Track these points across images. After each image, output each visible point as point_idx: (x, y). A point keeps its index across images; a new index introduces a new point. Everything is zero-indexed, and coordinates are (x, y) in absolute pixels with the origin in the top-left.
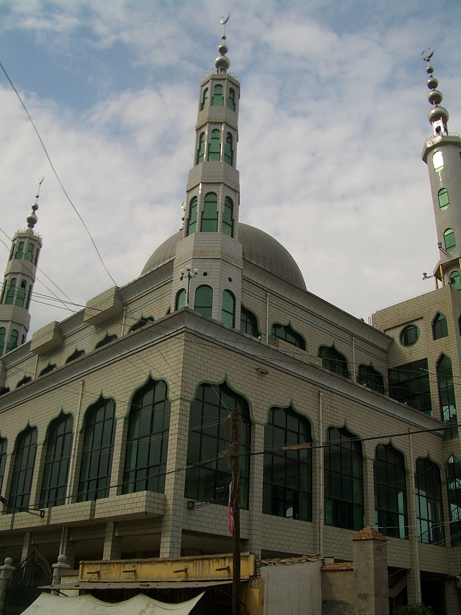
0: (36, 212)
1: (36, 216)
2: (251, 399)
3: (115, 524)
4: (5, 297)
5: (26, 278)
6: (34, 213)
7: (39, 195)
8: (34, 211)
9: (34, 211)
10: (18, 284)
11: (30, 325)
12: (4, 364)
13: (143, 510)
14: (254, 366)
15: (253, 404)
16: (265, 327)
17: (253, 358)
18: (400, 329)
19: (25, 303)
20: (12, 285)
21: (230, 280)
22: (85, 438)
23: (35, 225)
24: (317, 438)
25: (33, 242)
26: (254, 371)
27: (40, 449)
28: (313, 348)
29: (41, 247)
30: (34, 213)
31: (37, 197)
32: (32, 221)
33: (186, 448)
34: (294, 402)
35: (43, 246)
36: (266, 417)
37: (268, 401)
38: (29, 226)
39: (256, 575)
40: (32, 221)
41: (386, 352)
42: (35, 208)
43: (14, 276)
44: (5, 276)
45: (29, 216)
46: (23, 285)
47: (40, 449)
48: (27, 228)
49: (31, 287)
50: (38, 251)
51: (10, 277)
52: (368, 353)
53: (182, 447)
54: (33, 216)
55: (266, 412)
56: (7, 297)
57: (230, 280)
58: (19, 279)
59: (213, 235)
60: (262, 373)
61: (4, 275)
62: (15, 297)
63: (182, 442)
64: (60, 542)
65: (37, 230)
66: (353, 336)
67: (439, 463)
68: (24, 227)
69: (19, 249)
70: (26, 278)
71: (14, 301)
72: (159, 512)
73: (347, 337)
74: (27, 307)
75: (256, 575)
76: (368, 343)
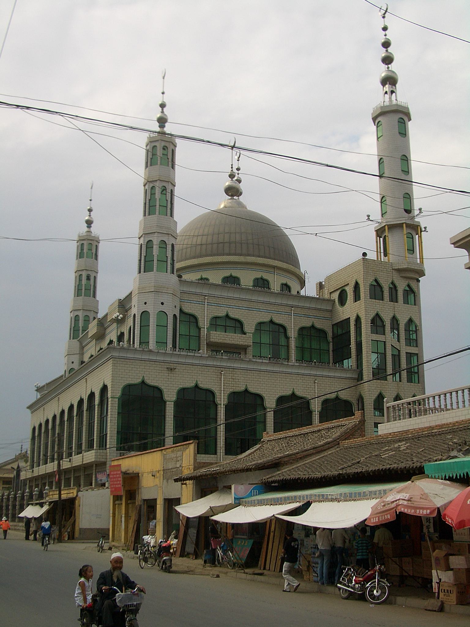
0: (165, 109)
1: (165, 115)
2: (162, 387)
3: (96, 465)
4: (147, 208)
5: (89, 273)
6: (162, 112)
7: (165, 91)
8: (162, 110)
9: (162, 110)
10: (158, 191)
13: (93, 460)
14: (165, 367)
16: (204, 323)
17: (164, 362)
18: (338, 292)
19: (169, 211)
21: (162, 304)
22: (101, 408)
24: (219, 402)
25: (90, 242)
26: (166, 369)
28: (249, 327)
29: (176, 146)
30: (162, 112)
31: (163, 93)
33: (116, 424)
34: (199, 382)
35: (178, 146)
36: (175, 396)
37: (177, 386)
38: (88, 227)
40: (89, 223)
41: (331, 311)
42: (163, 106)
43: (80, 273)
44: (144, 186)
48: (87, 229)
49: (172, 192)
50: (173, 152)
51: (149, 186)
53: (113, 424)
54: (163, 115)
55: (175, 393)
56: (150, 207)
57: (162, 304)
61: (143, 185)
63: (113, 421)
64: (71, 478)
65: (95, 229)
66: (292, 307)
67: (351, 399)
69: (153, 155)
70: (89, 273)
71: (157, 211)
72: (103, 460)
73: (287, 309)
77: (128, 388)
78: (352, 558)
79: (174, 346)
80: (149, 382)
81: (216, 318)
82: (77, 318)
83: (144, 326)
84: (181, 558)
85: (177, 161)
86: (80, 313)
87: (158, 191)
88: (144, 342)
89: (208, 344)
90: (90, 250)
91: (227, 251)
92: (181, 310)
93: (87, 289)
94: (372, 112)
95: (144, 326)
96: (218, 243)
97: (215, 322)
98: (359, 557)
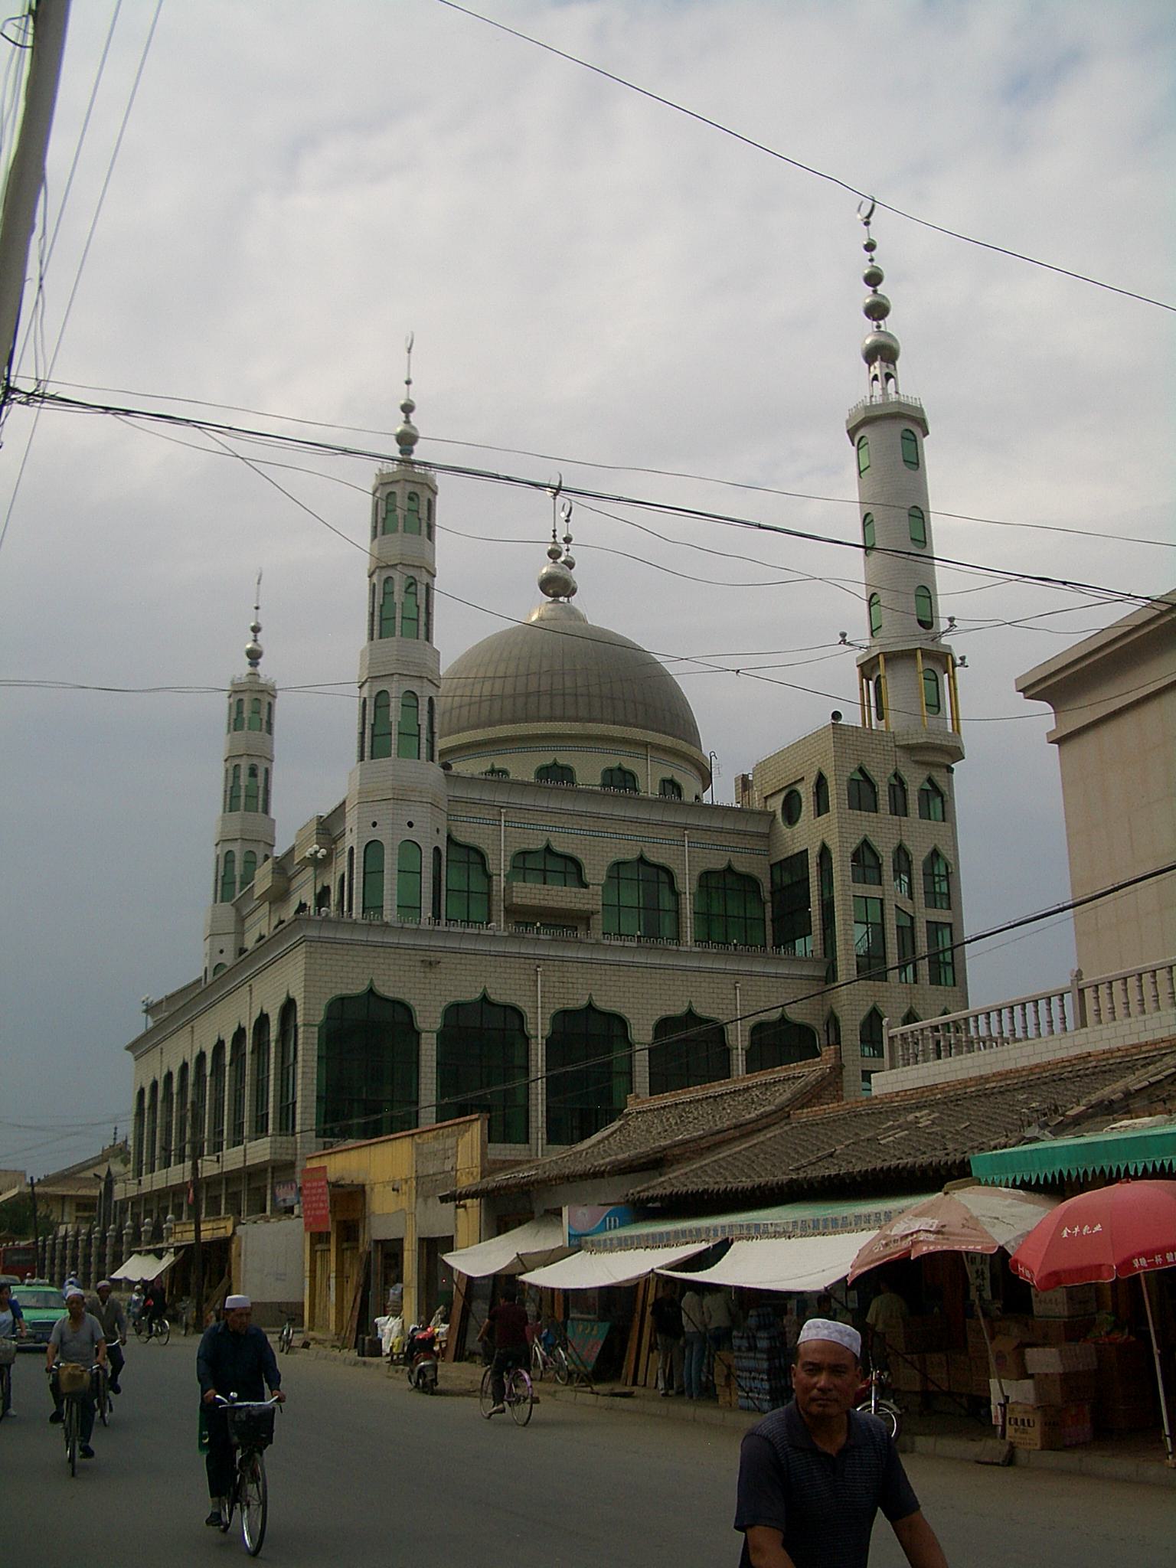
0: (412, 415)
1: (413, 428)
3: (208, 1184)
6: (407, 422)
8: (407, 417)
9: (407, 417)
10: (244, 772)
11: (276, 835)
12: (238, 910)
13: (267, 1158)
15: (417, 1008)
16: (500, 864)
18: (782, 796)
20: (388, 594)
21: (410, 825)
23: (415, 447)
24: (532, 1032)
27: (273, 1045)
28: (596, 872)
30: (407, 422)
31: (408, 383)
32: (254, 656)
38: (251, 664)
39: (234, 1233)
44: (370, 576)
45: (398, 430)
46: (253, 772)
47: (273, 1045)
52: (723, 848)
57: (410, 825)
58: (245, 764)
59: (384, 761)
60: (430, 963)
62: (398, 619)
68: (243, 667)
72: (289, 1158)
73: (674, 834)
74: (428, 638)
75: (234, 1233)
76: (721, 831)
77: (339, 1006)
79: (436, 914)
81: (524, 853)
82: (229, 857)
83: (373, 872)
86: (236, 848)
88: (373, 906)
93: (251, 796)
95: (373, 872)
97: (524, 863)
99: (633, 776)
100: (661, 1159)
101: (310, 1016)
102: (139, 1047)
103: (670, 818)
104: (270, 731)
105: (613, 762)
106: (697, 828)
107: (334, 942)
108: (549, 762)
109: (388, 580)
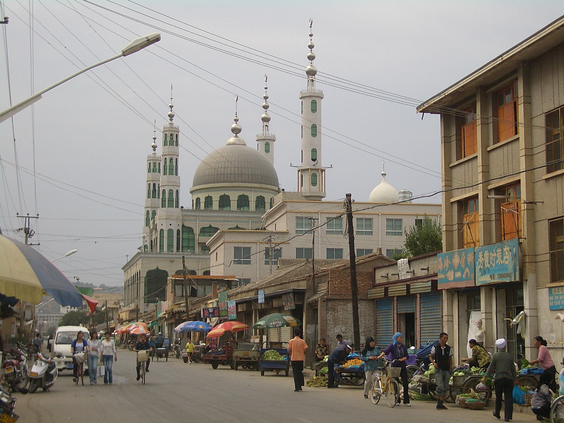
10: (168, 161)
16: (197, 231)
59: (164, 209)
73: (246, 220)
77: (149, 273)
78: (377, 375)
79: (178, 248)
80: (160, 268)
81: (204, 228)
82: (148, 212)
83: (162, 236)
84: (17, 297)
85: (179, 143)
86: (149, 209)
87: (168, 161)
88: (161, 247)
89: (199, 243)
90: (155, 166)
91: (222, 180)
92: (183, 226)
93: (171, 169)
94: (89, 283)
95: (162, 236)
96: (217, 175)
97: (204, 231)
98: (112, 321)
99: (247, 197)
100: (18, 330)
101: (144, 275)
102: (126, 268)
103: (245, 215)
104: (177, 145)
105: (241, 193)
106: (253, 217)
107: (148, 257)
108: (223, 194)
109: (166, 159)
